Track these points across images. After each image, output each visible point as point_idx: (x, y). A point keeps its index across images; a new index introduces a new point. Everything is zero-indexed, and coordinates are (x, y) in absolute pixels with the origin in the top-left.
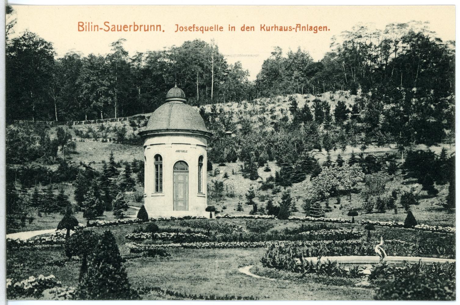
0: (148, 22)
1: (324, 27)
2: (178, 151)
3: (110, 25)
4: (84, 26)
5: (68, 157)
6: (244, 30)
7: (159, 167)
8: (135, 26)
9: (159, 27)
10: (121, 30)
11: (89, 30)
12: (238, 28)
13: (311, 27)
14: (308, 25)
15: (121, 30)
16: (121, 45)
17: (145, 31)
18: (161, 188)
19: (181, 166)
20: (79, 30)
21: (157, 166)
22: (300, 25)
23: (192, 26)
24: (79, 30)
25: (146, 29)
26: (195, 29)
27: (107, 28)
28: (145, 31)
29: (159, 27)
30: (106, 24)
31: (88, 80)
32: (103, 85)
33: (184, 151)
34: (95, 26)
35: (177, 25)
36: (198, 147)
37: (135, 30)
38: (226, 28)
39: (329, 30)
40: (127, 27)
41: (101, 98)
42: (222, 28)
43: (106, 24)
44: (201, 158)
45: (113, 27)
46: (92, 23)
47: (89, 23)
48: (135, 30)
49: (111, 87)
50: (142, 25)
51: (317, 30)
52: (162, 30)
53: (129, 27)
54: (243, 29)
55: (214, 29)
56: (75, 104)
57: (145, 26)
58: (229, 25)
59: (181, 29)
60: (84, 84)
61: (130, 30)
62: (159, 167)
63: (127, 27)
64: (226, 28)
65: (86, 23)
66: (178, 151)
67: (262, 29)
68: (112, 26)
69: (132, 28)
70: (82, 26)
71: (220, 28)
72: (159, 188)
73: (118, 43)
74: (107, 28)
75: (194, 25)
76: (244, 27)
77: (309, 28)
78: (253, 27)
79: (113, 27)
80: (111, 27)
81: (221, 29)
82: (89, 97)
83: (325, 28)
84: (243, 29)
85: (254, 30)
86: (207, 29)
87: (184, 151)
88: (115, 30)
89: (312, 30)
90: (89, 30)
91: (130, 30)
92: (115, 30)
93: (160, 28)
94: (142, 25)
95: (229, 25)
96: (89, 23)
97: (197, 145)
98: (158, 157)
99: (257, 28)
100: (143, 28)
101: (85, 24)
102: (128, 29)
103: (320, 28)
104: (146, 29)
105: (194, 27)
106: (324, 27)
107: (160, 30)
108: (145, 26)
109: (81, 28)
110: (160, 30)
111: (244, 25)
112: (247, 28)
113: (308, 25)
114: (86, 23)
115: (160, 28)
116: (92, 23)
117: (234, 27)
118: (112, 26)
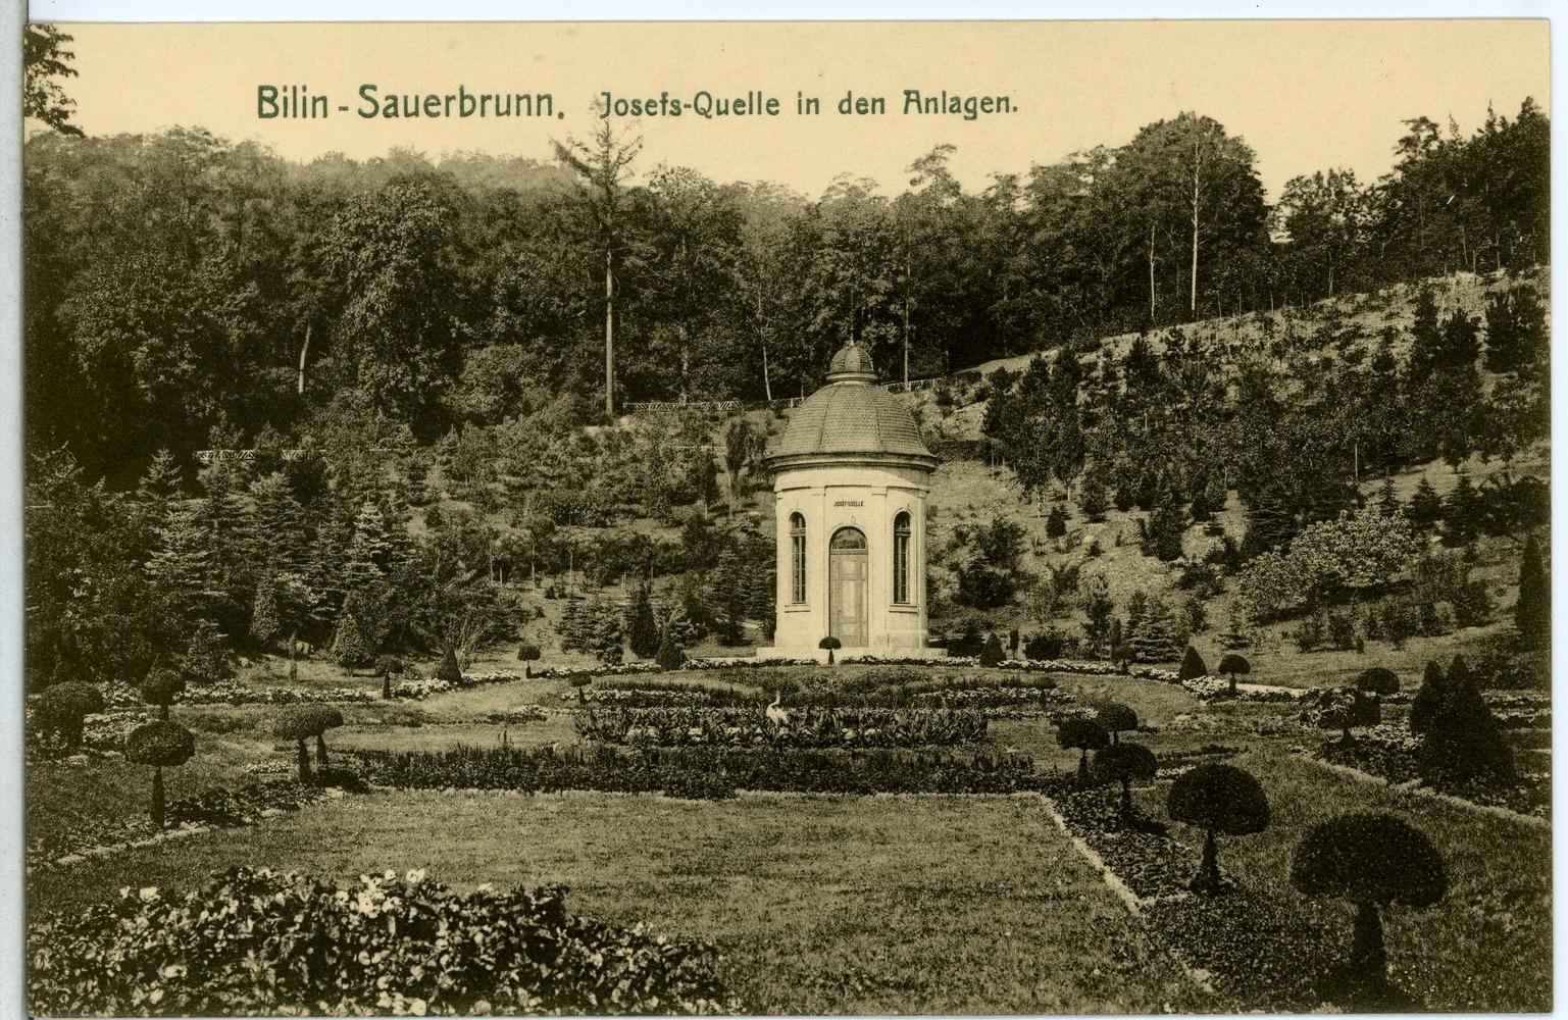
0: (506, 88)
1: (999, 100)
2: (838, 504)
3: (379, 96)
4: (279, 101)
5: (749, 501)
6: (849, 111)
7: (800, 542)
8: (463, 98)
9: (545, 103)
10: (416, 114)
11: (305, 115)
12: (829, 106)
13: (957, 100)
14: (944, 94)
15: (416, 114)
16: (943, 164)
17: (498, 114)
18: (904, 596)
19: (848, 540)
20: (261, 115)
21: (796, 540)
22: (917, 93)
23: (658, 98)
24: (261, 115)
25: (503, 108)
26: (669, 107)
27: (369, 108)
28: (498, 114)
29: (813, 105)
30: (368, 92)
31: (832, 280)
32: (873, 291)
33: (853, 504)
34: (315, 100)
35: (608, 95)
36: (891, 492)
37: (463, 114)
38: (788, 106)
39: (1015, 109)
40: (439, 103)
41: (868, 329)
42: (777, 104)
43: (368, 92)
44: (902, 519)
45: (390, 101)
46: (304, 89)
47: (295, 89)
48: (463, 114)
49: (893, 295)
50: (489, 97)
51: (974, 111)
52: (555, 112)
53: (995, 101)
54: (845, 107)
55: (747, 108)
56: (801, 351)
57: (498, 97)
58: (800, 94)
59: (621, 108)
60: (822, 293)
61: (447, 114)
62: (800, 542)
63: (439, 103)
64: (788, 106)
65: (285, 89)
66: (838, 504)
67: (913, 106)
68: (387, 98)
69: (455, 106)
70: (271, 101)
71: (768, 105)
72: (800, 595)
73: (932, 158)
74: (369, 108)
75: (664, 95)
76: (849, 100)
77: (949, 104)
78: (882, 100)
79: (390, 101)
80: (383, 104)
81: (773, 109)
82: (836, 328)
83: (1003, 104)
84: (845, 107)
85: (882, 112)
86: (723, 108)
87: (853, 504)
88: (396, 114)
89: (959, 111)
90: (305, 115)
91: (447, 114)
92: (396, 114)
93: (497, 106)
94: (489, 97)
95: (800, 94)
96: (295, 89)
97: (889, 487)
98: (797, 518)
99: (895, 103)
100: (490, 105)
101: (281, 95)
102: (442, 109)
103: (987, 101)
104: (503, 108)
105: (664, 102)
106: (999, 100)
107: (550, 113)
108: (498, 97)
109: (268, 108)
110: (550, 113)
111: (850, 93)
112: (858, 105)
113: (944, 94)
114: (285, 89)
115: (497, 106)
116: (304, 89)
117: (816, 101)
118: (387, 98)
